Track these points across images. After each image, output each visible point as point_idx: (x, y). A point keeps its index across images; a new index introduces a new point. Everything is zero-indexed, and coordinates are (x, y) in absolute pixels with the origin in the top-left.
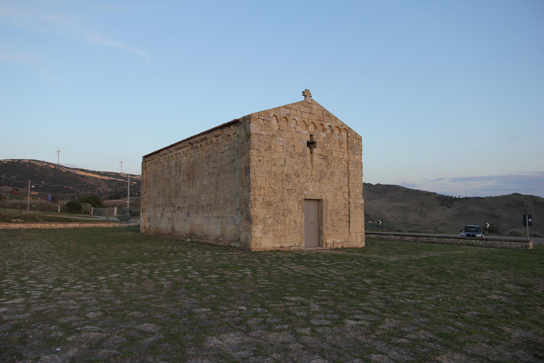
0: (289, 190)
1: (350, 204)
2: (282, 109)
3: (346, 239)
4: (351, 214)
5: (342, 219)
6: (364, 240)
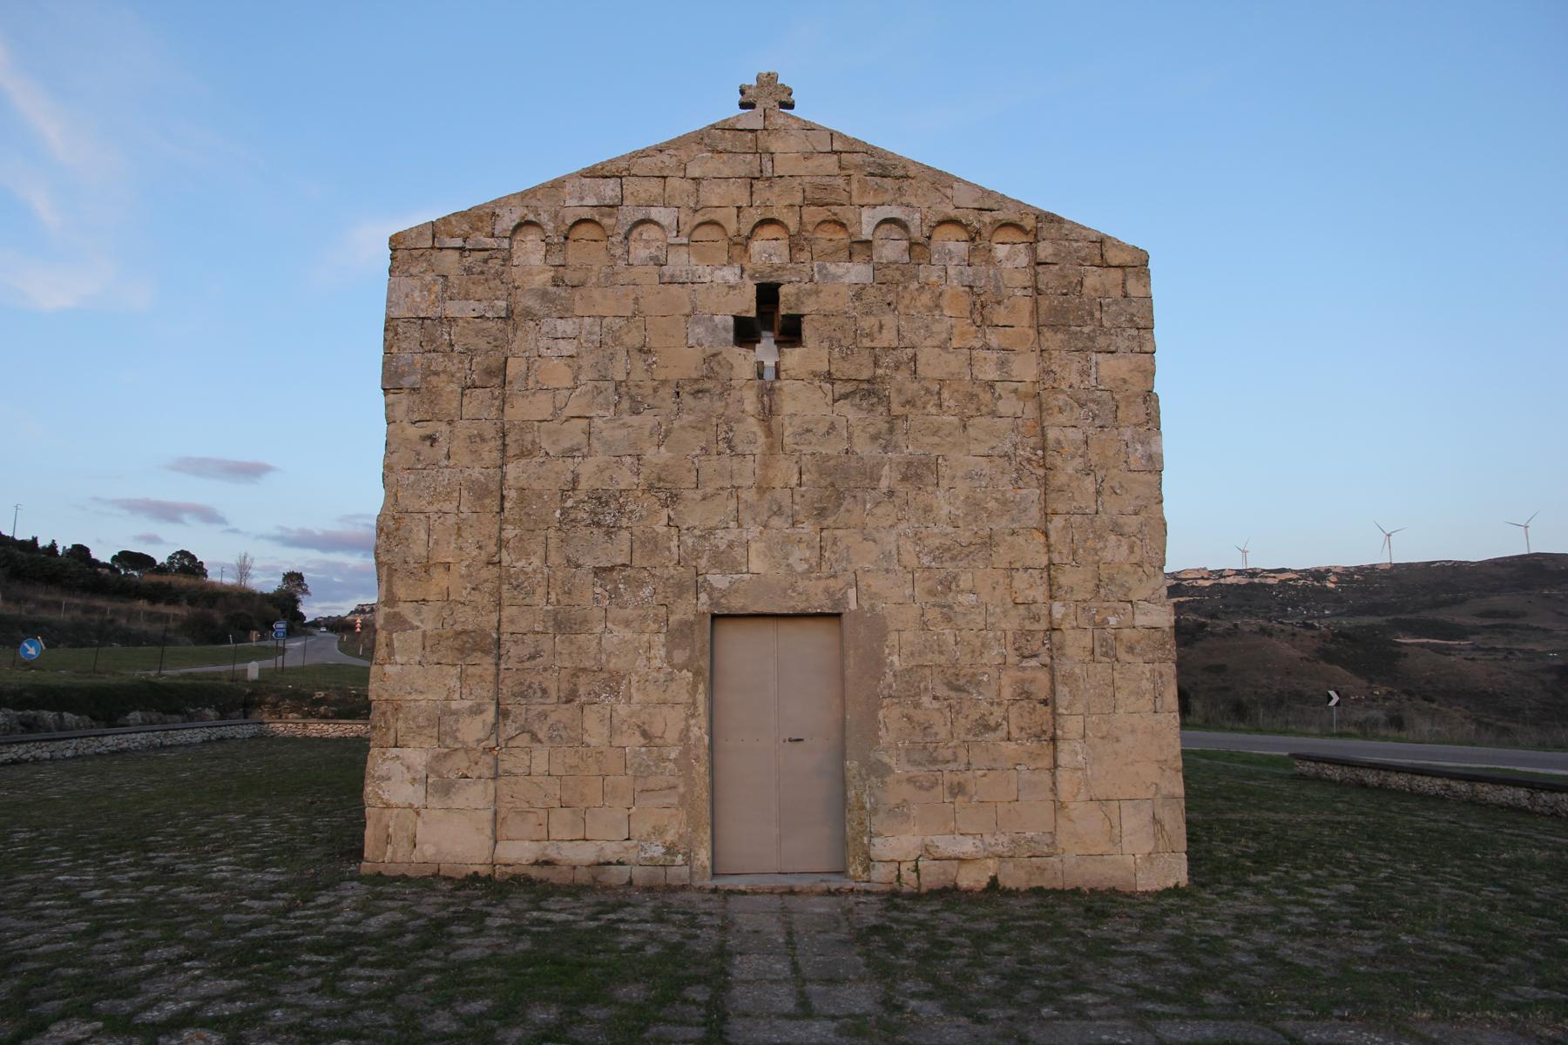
1: (1056, 636)
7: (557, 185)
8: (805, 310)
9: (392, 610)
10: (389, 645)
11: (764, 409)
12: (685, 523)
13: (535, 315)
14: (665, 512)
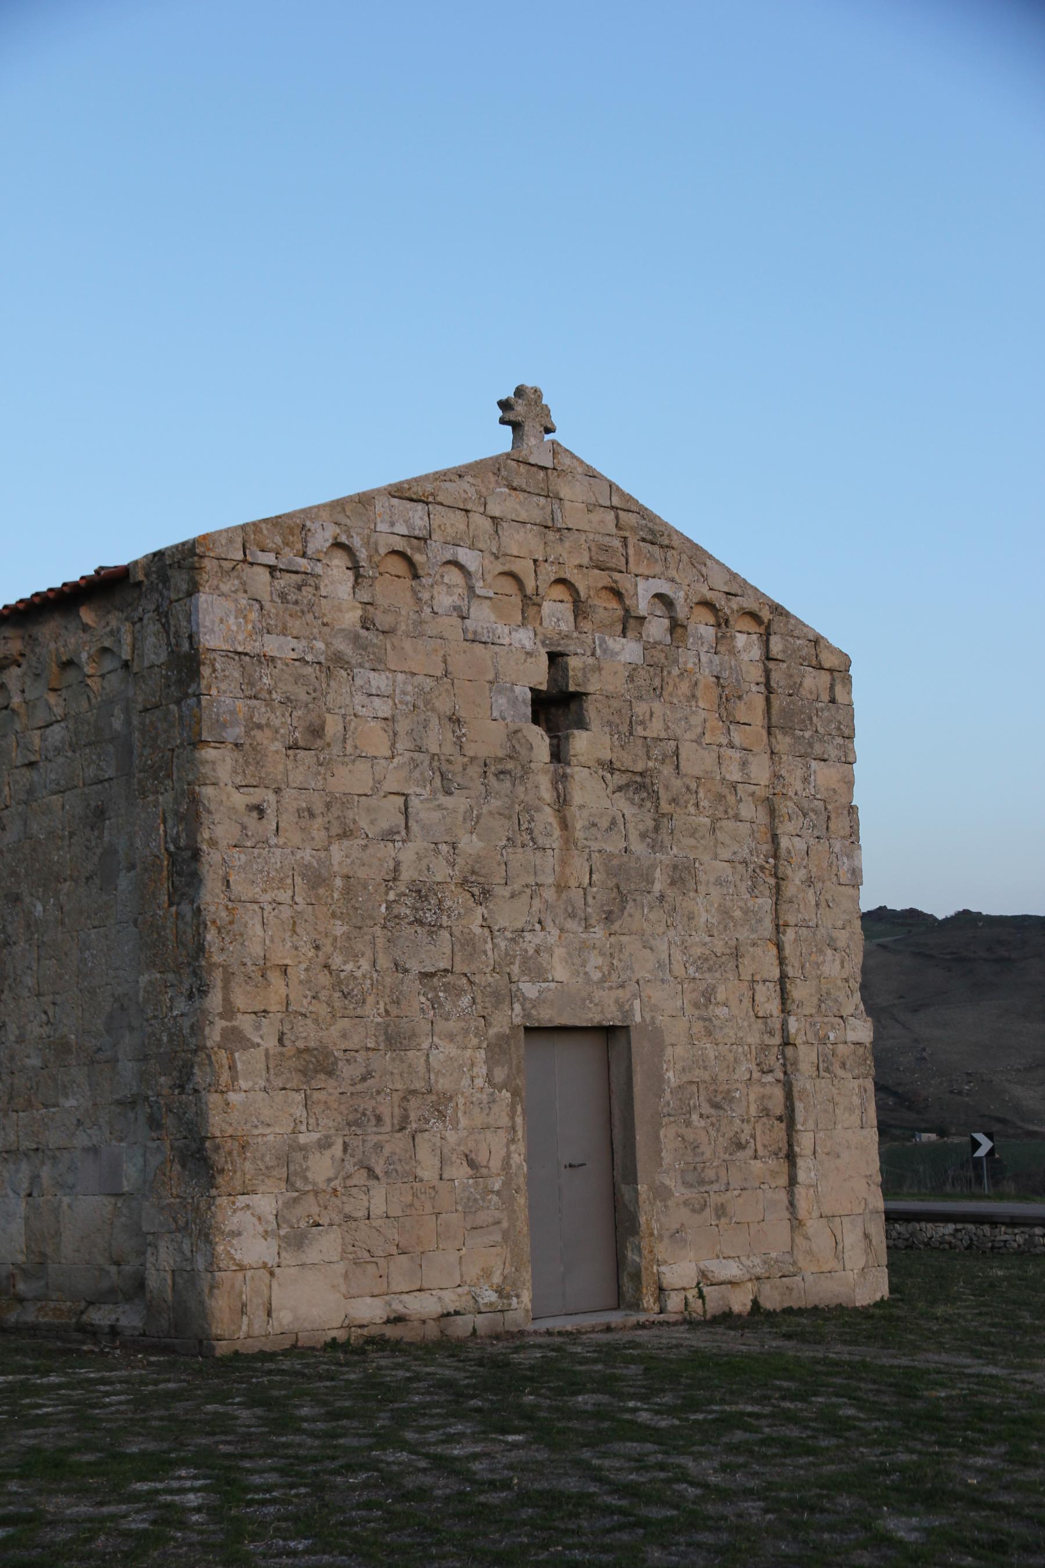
0: (432, 975)
1: (789, 1051)
2: (381, 505)
3: (773, 1255)
4: (799, 1106)
5: (744, 1137)
6: (884, 1260)
7: (365, 500)
8: (591, 689)
9: (229, 1024)
10: (232, 1068)
11: (558, 797)
12: (496, 924)
13: (348, 663)
14: (480, 910)
